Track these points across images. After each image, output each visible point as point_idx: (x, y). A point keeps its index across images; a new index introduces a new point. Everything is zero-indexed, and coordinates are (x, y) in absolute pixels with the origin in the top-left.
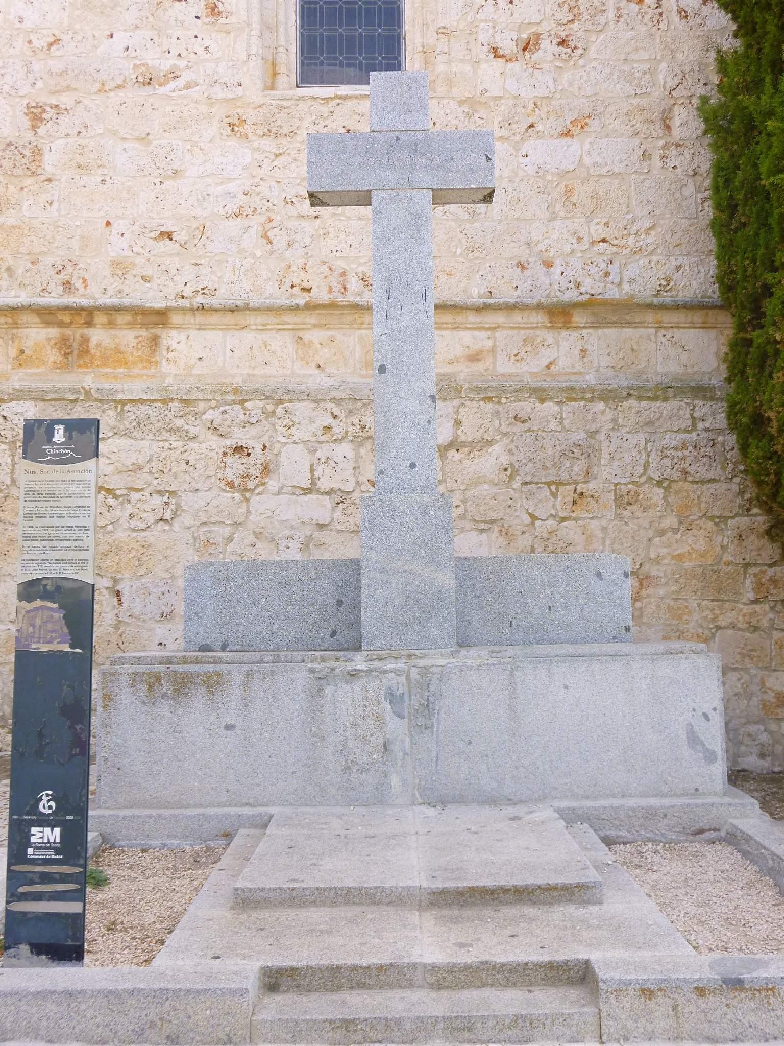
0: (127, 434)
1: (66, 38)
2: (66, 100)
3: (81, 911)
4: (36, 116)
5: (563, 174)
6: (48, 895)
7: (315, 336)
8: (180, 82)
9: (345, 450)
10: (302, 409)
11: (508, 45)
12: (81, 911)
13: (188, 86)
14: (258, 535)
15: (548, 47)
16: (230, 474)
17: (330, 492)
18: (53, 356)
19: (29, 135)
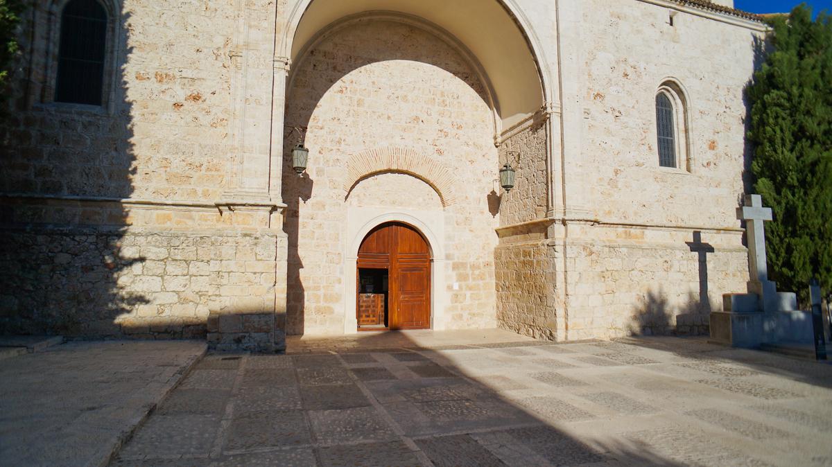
0: (644, 257)
1: (716, 137)
2: (622, 168)
3: (277, 299)
4: (616, 172)
5: (717, 196)
6: (292, 303)
7: (674, 233)
8: (644, 166)
9: (685, 262)
10: (677, 252)
11: (705, 164)
12: (277, 299)
13: (646, 167)
14: (670, 282)
15: (712, 165)
16: (665, 267)
17: (682, 272)
18: (624, 235)
19: (615, 177)
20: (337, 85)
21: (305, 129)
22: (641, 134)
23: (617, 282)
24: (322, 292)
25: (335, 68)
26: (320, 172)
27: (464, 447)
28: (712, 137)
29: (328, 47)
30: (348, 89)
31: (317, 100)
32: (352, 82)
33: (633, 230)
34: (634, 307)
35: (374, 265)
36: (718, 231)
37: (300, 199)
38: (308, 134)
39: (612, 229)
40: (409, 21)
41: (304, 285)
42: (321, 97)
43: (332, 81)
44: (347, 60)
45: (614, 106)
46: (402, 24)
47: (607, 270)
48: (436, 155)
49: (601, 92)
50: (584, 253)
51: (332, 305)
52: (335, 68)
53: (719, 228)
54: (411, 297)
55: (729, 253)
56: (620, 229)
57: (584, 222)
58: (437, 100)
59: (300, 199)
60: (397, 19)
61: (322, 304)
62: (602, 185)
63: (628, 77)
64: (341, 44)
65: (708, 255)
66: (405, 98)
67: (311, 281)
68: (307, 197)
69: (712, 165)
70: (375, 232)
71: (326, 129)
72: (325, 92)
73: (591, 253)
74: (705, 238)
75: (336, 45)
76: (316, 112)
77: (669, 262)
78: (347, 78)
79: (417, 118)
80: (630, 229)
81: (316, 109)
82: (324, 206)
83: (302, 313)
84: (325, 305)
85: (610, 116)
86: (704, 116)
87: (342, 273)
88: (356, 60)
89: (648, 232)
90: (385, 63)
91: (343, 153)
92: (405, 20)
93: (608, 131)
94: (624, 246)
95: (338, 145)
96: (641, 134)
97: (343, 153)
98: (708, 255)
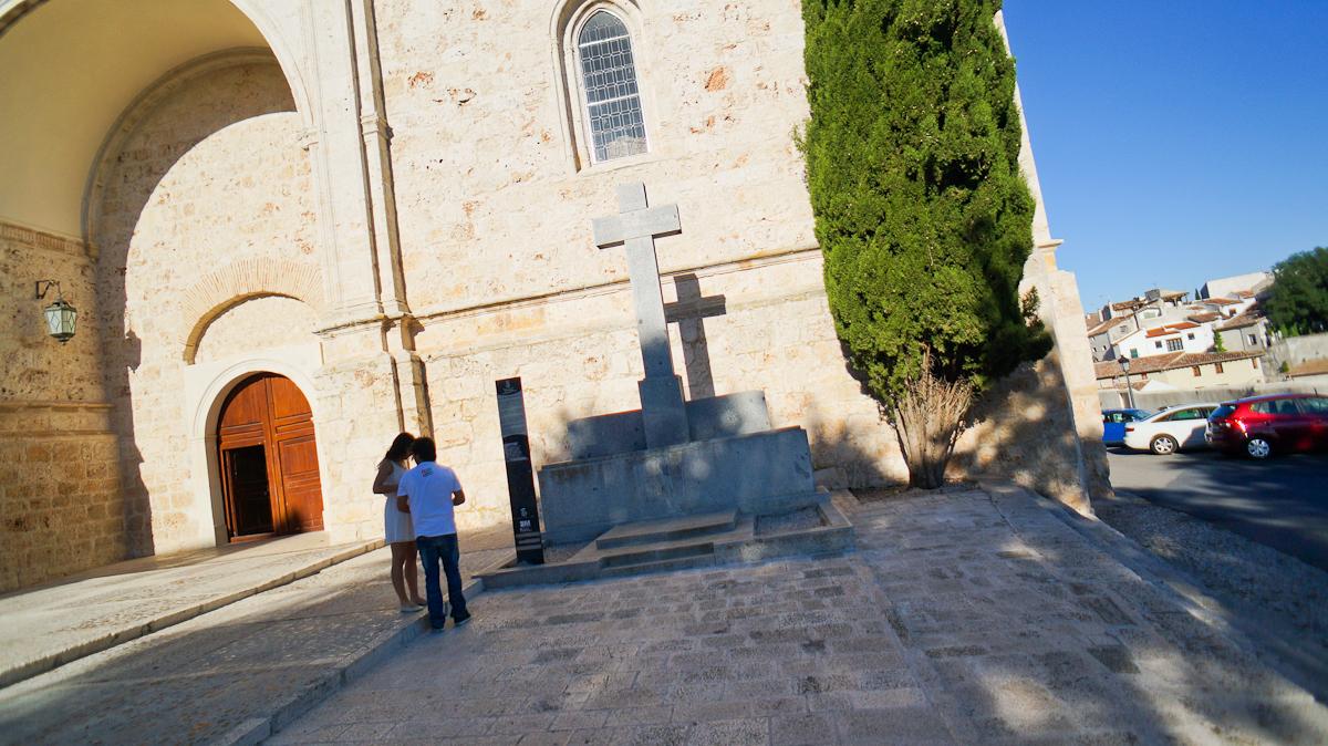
1: (726, 59)
2: (480, 198)
4: (468, 210)
8: (535, 178)
15: (720, 123)
18: (494, 327)
20: (154, 197)
21: (123, 271)
22: (523, 117)
23: (474, 421)
24: (170, 492)
25: (150, 171)
26: (148, 325)
27: (616, 724)
28: (713, 62)
29: (138, 144)
30: (171, 195)
31: (133, 225)
32: (174, 183)
33: (515, 312)
34: (880, 452)
35: (244, 442)
36: (746, 265)
37: (129, 368)
38: (128, 277)
39: (463, 320)
40: (234, 60)
41: (148, 485)
42: (137, 218)
43: (149, 192)
44: (165, 153)
45: (455, 85)
46: (233, 68)
47: (451, 402)
48: (302, 254)
49: (425, 68)
50: (357, 384)
51: (183, 510)
52: (150, 171)
53: (747, 255)
54: (302, 483)
55: (770, 309)
56: (485, 317)
57: (363, 326)
58: (296, 168)
59: (129, 368)
60: (220, 63)
61: (172, 510)
62: (439, 243)
63: (484, 16)
64: (153, 133)
65: (709, 324)
66: (248, 183)
67: (155, 481)
68: (136, 365)
69: (720, 123)
70: (240, 394)
71: (150, 263)
72: (141, 209)
73: (372, 381)
74: (708, 287)
75: (148, 136)
76: (134, 242)
77: (600, 360)
78: (166, 180)
79: (269, 205)
80: (509, 312)
81: (134, 237)
82: (158, 373)
83: (149, 525)
84: (176, 510)
85: (450, 106)
86: (685, 24)
87: (190, 462)
88: (176, 148)
89: (551, 307)
90: (213, 138)
91: (173, 290)
92: (230, 59)
93: (445, 137)
94: (481, 349)
95: (165, 280)
96: (523, 117)
97: (173, 290)
98: (709, 324)
